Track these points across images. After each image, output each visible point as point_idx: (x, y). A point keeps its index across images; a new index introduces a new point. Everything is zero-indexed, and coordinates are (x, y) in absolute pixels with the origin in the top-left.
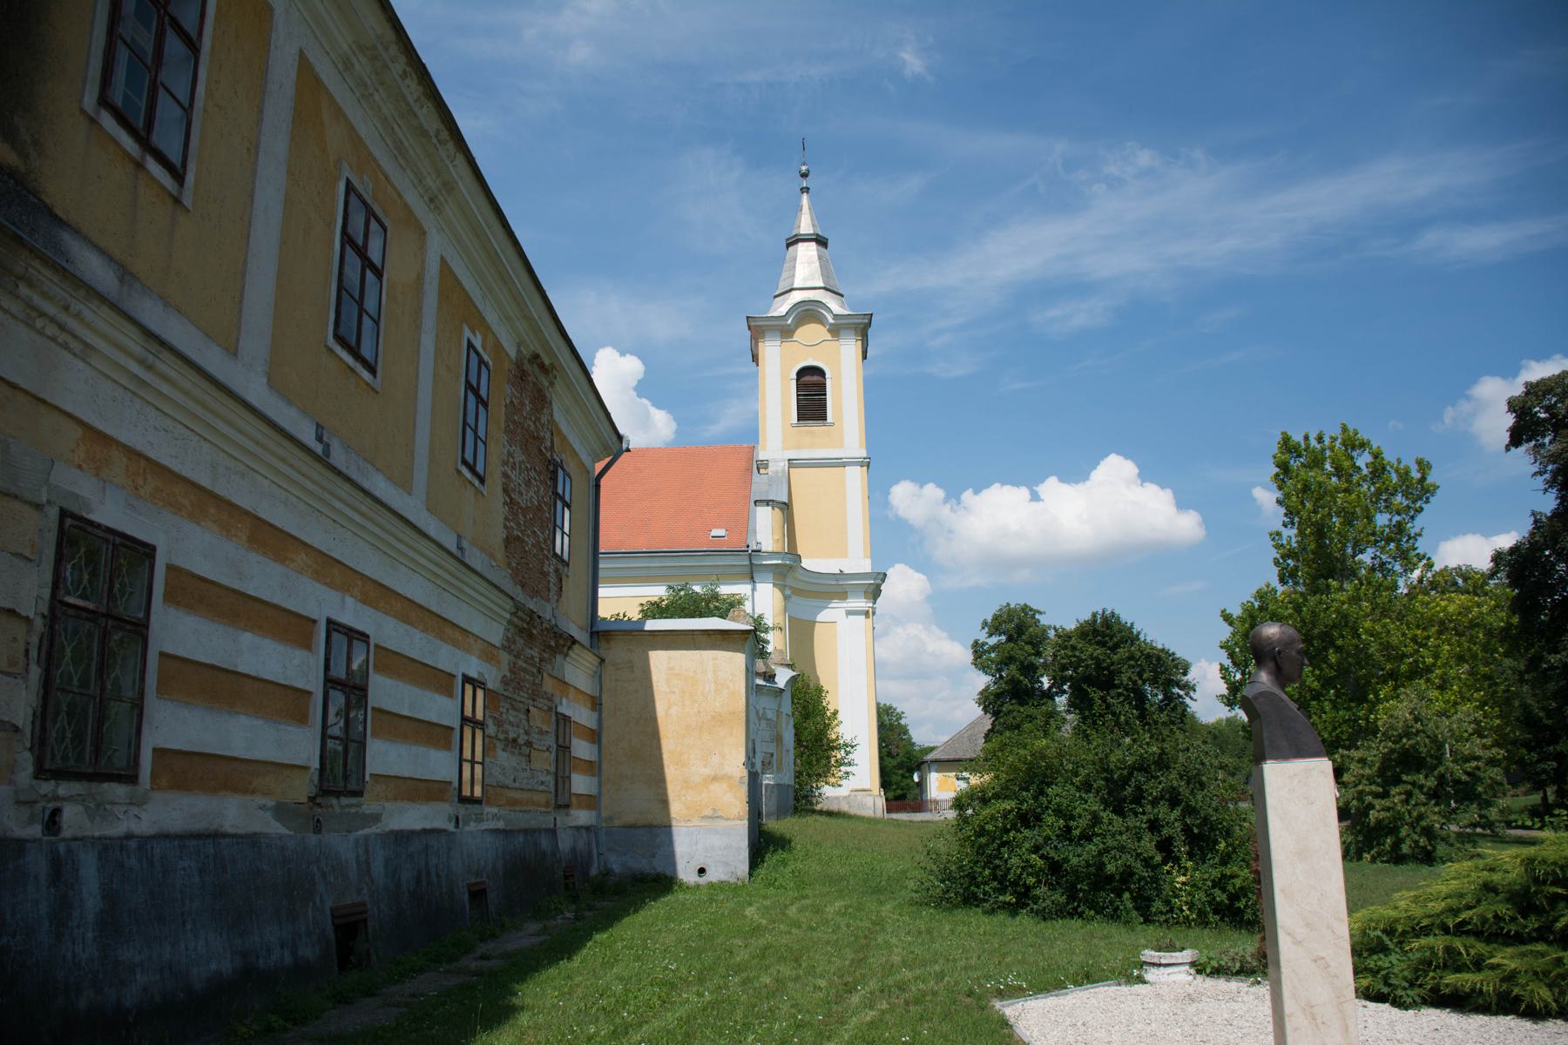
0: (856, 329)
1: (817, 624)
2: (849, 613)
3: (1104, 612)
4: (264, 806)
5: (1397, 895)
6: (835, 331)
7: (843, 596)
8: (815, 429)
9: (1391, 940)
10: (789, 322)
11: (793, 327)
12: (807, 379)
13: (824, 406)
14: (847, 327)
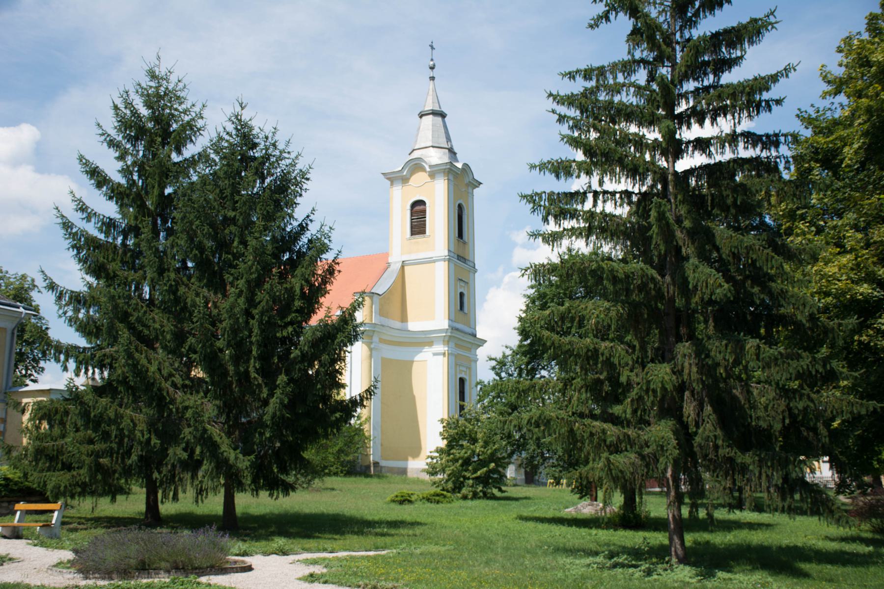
0: (444, 172)
1: (415, 363)
2: (435, 354)
3: (96, 176)
4: (311, 575)
5: (690, 431)
6: (432, 175)
7: (430, 344)
8: (419, 239)
9: (67, 421)
10: (405, 173)
11: (408, 176)
12: (418, 208)
13: (425, 225)
14: (439, 172)
